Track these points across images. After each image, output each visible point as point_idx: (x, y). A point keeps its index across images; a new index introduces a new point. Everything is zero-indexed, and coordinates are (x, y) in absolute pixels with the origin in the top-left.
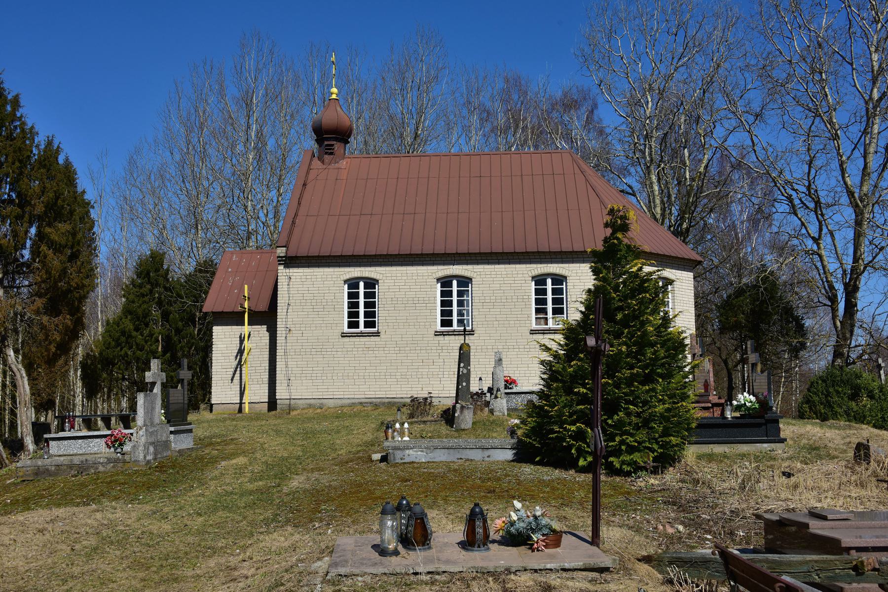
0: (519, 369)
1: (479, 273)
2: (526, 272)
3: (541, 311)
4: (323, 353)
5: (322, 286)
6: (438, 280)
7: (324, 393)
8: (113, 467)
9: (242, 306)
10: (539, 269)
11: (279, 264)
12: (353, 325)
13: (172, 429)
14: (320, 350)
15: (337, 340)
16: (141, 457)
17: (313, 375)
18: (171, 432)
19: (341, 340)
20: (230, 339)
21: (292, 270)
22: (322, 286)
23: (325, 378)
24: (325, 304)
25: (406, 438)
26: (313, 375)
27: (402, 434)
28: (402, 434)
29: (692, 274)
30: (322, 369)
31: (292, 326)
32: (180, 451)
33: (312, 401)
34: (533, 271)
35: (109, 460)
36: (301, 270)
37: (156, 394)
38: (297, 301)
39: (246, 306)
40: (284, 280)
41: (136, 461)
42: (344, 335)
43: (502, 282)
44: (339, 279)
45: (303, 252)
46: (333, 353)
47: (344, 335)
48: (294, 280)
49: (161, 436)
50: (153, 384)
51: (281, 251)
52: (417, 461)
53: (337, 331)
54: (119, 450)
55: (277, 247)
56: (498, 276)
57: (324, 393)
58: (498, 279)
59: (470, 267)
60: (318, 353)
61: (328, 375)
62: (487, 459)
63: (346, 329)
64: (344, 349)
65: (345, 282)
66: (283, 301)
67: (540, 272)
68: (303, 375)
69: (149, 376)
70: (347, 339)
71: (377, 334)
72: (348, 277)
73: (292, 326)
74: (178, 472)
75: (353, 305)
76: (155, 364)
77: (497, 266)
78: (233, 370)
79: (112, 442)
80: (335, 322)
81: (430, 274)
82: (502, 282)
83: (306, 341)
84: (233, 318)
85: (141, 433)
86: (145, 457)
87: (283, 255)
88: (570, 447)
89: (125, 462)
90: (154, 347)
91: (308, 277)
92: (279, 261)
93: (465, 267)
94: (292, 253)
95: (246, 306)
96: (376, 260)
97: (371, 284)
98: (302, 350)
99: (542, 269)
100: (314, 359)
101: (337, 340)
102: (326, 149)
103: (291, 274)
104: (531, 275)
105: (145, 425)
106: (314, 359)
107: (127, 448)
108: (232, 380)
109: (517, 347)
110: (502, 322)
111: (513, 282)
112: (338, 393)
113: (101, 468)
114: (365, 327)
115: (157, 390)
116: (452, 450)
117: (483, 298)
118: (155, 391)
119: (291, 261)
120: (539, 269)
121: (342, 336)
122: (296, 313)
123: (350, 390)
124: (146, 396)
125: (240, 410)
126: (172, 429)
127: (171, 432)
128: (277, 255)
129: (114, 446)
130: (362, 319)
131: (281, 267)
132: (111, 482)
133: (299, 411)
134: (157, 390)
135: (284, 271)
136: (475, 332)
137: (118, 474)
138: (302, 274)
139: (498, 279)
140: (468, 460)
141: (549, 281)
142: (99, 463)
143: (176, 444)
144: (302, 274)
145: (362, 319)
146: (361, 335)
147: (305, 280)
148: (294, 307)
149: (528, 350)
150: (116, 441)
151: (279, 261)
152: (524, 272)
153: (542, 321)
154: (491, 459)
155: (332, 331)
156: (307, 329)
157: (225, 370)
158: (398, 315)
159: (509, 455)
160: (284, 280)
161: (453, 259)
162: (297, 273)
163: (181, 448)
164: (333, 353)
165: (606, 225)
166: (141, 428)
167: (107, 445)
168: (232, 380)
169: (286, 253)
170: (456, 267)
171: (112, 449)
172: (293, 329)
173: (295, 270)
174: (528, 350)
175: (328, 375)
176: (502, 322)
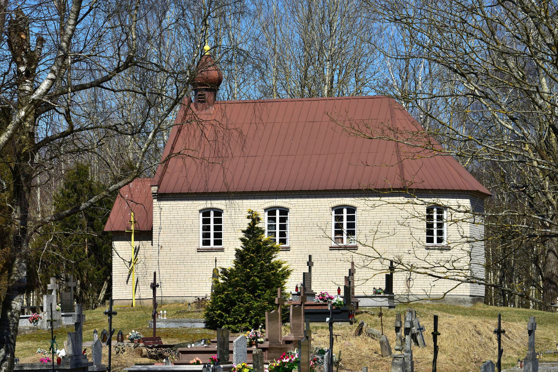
0: (321, 276)
1: (294, 205)
2: (327, 204)
3: (339, 232)
4: (184, 264)
5: (184, 214)
6: (265, 210)
7: (185, 293)
8: (32, 332)
9: (129, 229)
10: (337, 202)
11: (154, 198)
12: (206, 243)
13: (63, 314)
14: (182, 261)
15: (194, 254)
16: (46, 327)
17: (178, 279)
18: (62, 316)
19: (197, 254)
20: (125, 251)
21: (162, 203)
22: (184, 214)
23: (186, 282)
24: (186, 227)
25: (165, 318)
26: (178, 279)
27: (163, 316)
28: (163, 316)
29: (469, 200)
30: (184, 275)
31: (163, 244)
32: (67, 326)
33: (177, 298)
34: (332, 203)
35: (31, 328)
36: (169, 203)
37: (53, 295)
38: (166, 226)
39: (132, 228)
40: (157, 210)
41: (43, 329)
42: (199, 250)
43: (310, 212)
44: (195, 209)
45: (170, 190)
46: (192, 264)
47: (199, 250)
48: (164, 210)
49: (57, 317)
50: (51, 291)
51: (154, 189)
52: (162, 327)
53: (195, 248)
54: (36, 324)
55: (152, 186)
56: (307, 207)
57: (185, 293)
58: (307, 209)
59: (287, 200)
60: (181, 264)
61: (188, 279)
62: (193, 327)
63: (201, 246)
64: (199, 261)
65: (200, 211)
66: (157, 226)
67: (337, 204)
68: (170, 280)
69: (49, 287)
70: (201, 254)
71: (222, 250)
72: (202, 207)
73: (163, 244)
74: (63, 334)
75: (206, 228)
76: (52, 281)
77: (307, 200)
78: (127, 274)
79: (32, 320)
80: (193, 241)
81: (260, 206)
82: (310, 212)
83: (173, 255)
84: (124, 236)
85: (45, 315)
86: (47, 327)
87: (156, 192)
88: (218, 320)
89: (38, 329)
90: (80, 250)
91: (174, 208)
92: (153, 196)
93: (284, 200)
94: (161, 191)
95: (132, 228)
96: (221, 195)
97: (218, 213)
98: (170, 261)
99: (339, 201)
100: (179, 268)
101: (194, 254)
102: (199, 98)
103: (161, 206)
104: (331, 206)
105: (47, 311)
106: (179, 268)
107: (39, 323)
108: (127, 282)
109: (320, 259)
110: (310, 241)
111: (318, 211)
112: (195, 293)
113: (27, 332)
114: (214, 245)
115: (54, 293)
116: (177, 323)
117: (297, 223)
118: (53, 294)
119: (162, 197)
120: (337, 202)
121: (198, 252)
122: (166, 235)
123: (203, 290)
124: (47, 296)
125: (132, 306)
126: (63, 314)
127: (62, 316)
128: (152, 192)
129: (33, 322)
130: (212, 239)
131: (155, 201)
132: (30, 337)
133: (167, 305)
134: (54, 293)
135: (157, 203)
136: (291, 248)
137: (34, 335)
138: (170, 206)
139: (307, 209)
140: (184, 327)
141: (345, 211)
142: (26, 330)
143: (66, 322)
144: (170, 206)
145: (212, 239)
146: (211, 250)
147: (172, 210)
148: (164, 230)
149: (328, 262)
150: (34, 319)
151: (153, 196)
152: (326, 204)
153: (340, 240)
154: (195, 327)
155: (190, 248)
156: (173, 246)
157: (121, 275)
158: (229, 236)
159: (203, 325)
160: (157, 210)
161: (276, 194)
162: (166, 205)
163: (69, 324)
164: (192, 264)
165: (248, 217)
166: (45, 313)
167: (30, 321)
168: (127, 282)
169: (157, 191)
170: (278, 200)
171: (33, 323)
172: (164, 246)
173: (165, 203)
174: (328, 262)
175: (188, 279)
176: (310, 241)
